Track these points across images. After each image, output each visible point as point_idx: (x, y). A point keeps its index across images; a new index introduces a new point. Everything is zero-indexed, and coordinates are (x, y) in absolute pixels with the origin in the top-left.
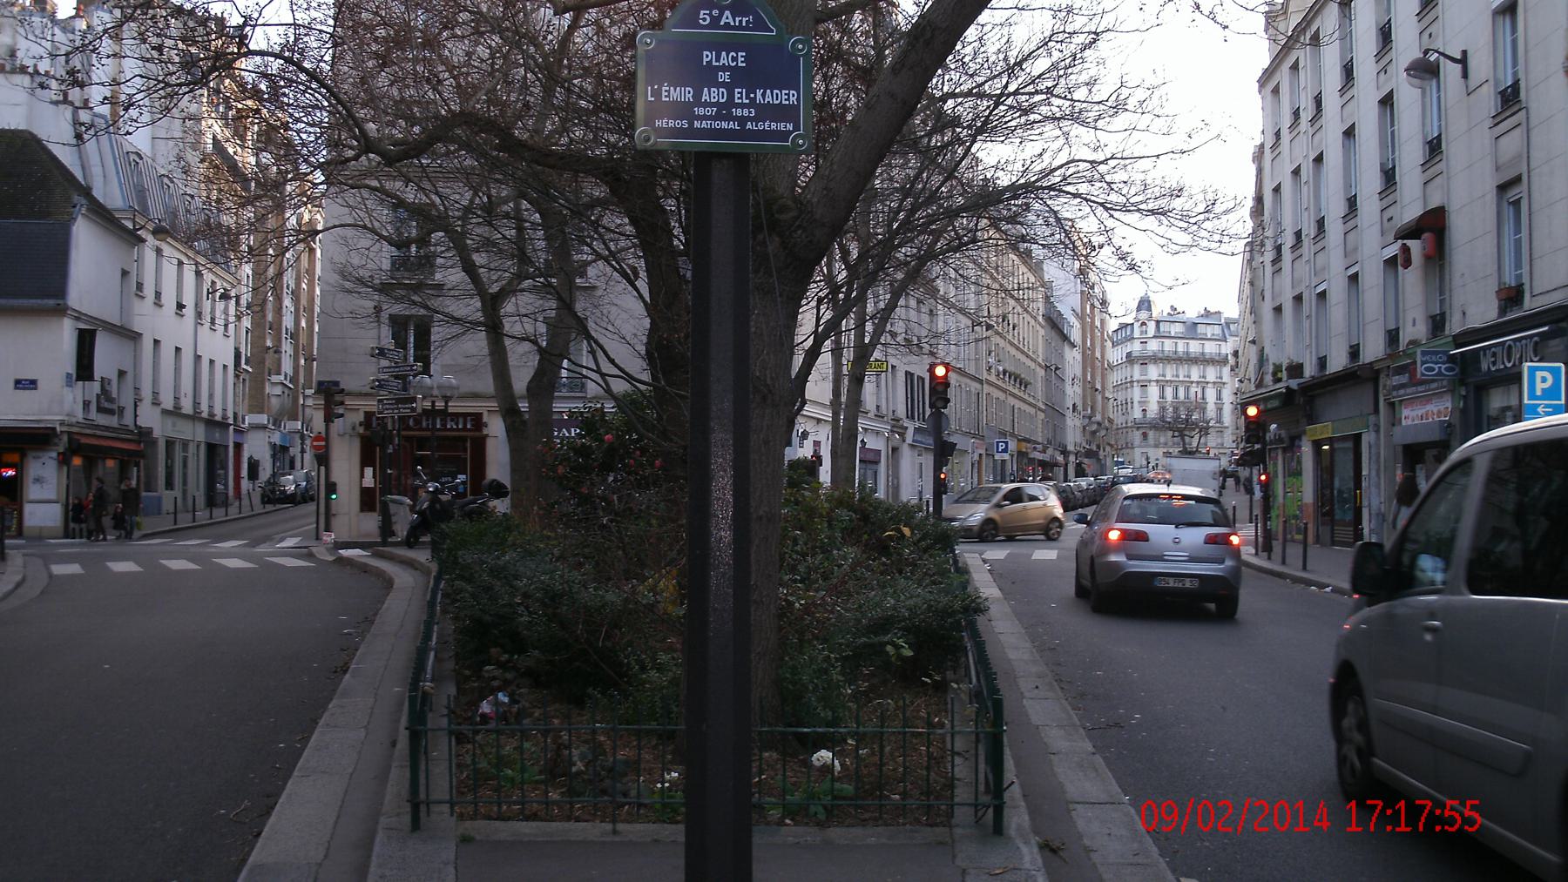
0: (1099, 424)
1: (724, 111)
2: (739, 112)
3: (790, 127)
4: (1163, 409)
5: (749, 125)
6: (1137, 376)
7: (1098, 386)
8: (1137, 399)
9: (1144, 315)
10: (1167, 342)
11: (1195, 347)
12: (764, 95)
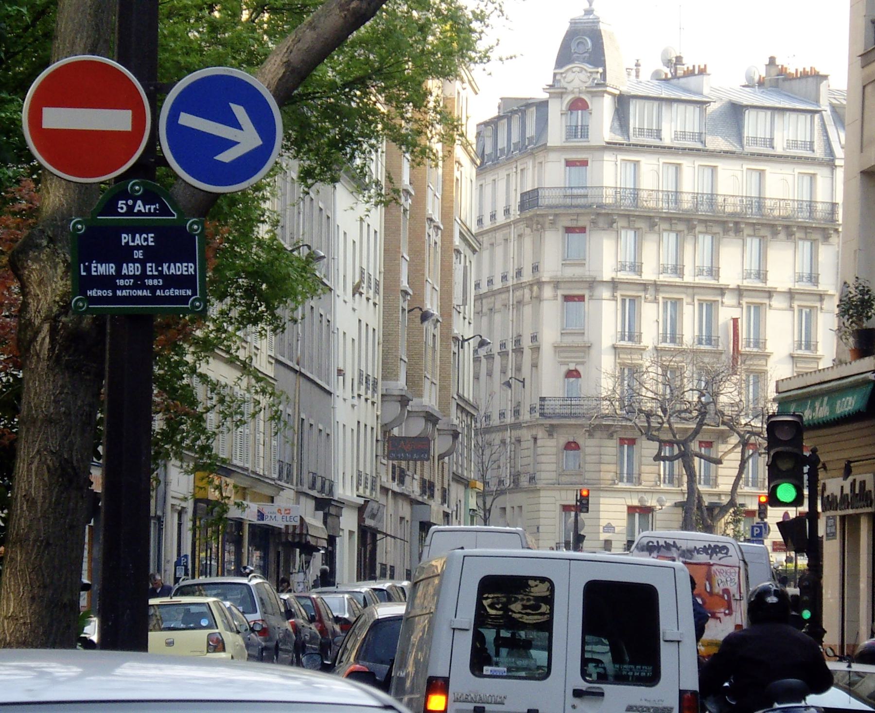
0: (430, 418)
1: (139, 281)
2: (149, 282)
3: (189, 293)
4: (630, 373)
5: (158, 293)
6: (552, 265)
7: (432, 305)
8: (549, 336)
9: (578, 78)
10: (649, 164)
11: (732, 183)
12: (169, 268)
